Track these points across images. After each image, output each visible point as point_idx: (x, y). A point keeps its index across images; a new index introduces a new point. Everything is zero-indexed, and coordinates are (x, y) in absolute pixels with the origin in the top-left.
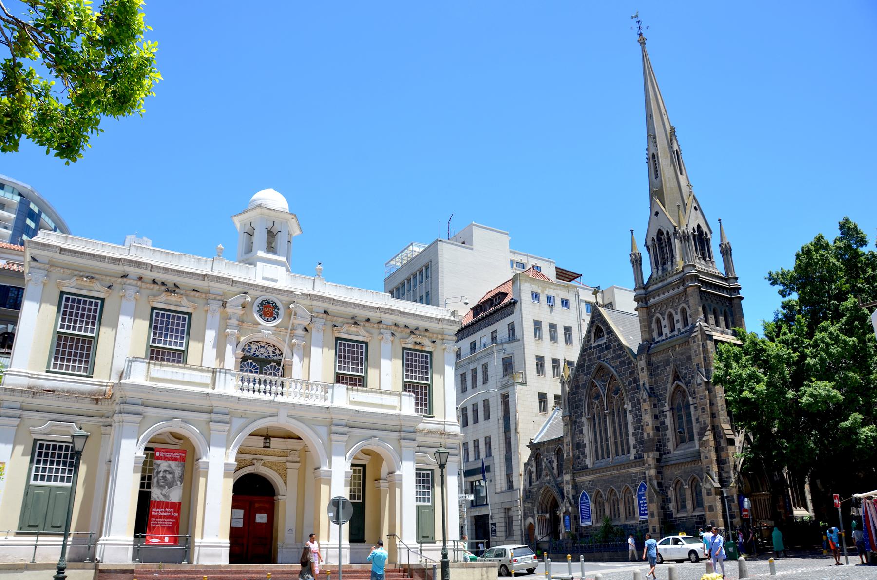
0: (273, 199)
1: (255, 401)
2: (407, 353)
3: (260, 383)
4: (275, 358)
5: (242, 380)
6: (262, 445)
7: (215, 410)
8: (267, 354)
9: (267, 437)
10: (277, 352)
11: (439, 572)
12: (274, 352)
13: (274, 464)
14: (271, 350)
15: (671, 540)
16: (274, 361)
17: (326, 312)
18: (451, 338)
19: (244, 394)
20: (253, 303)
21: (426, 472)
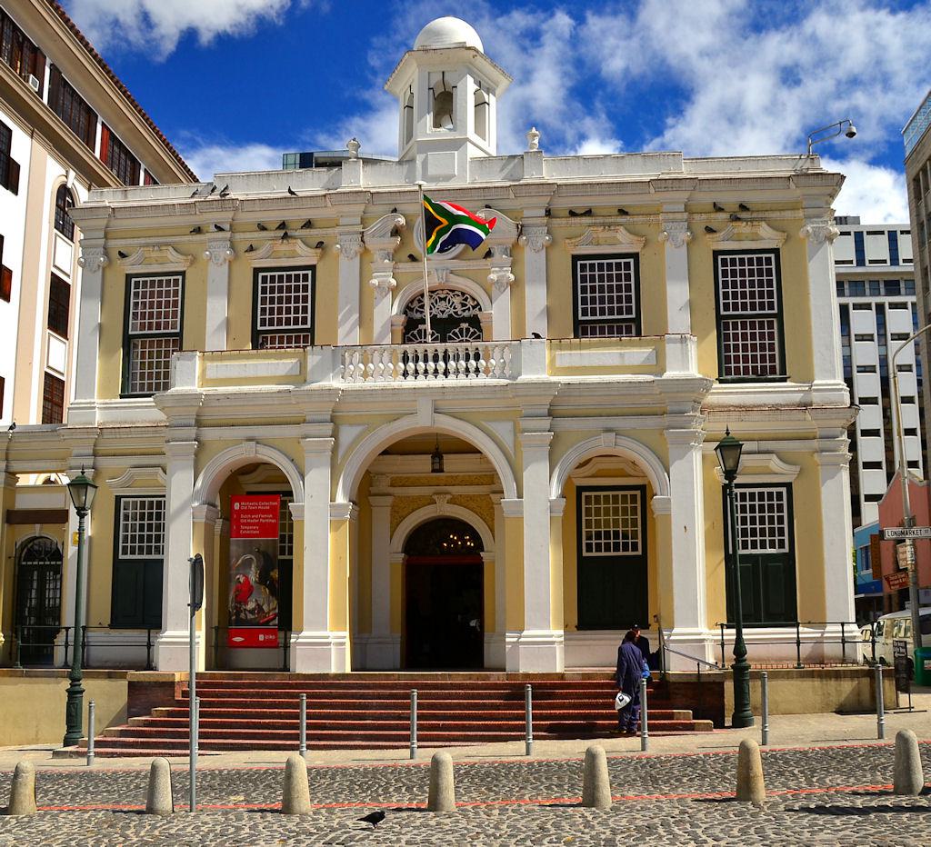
0: (458, 30)
1: (372, 392)
2: (583, 267)
3: (436, 359)
4: (466, 314)
5: (405, 360)
6: (429, 468)
7: (307, 418)
8: (452, 311)
9: (437, 455)
10: (470, 303)
11: (729, 686)
12: (464, 305)
13: (471, 498)
14: (457, 301)
15: (520, 678)
16: (464, 320)
17: (622, 212)
18: (538, 221)
19: (410, 383)
20: (409, 224)
21: (774, 490)
